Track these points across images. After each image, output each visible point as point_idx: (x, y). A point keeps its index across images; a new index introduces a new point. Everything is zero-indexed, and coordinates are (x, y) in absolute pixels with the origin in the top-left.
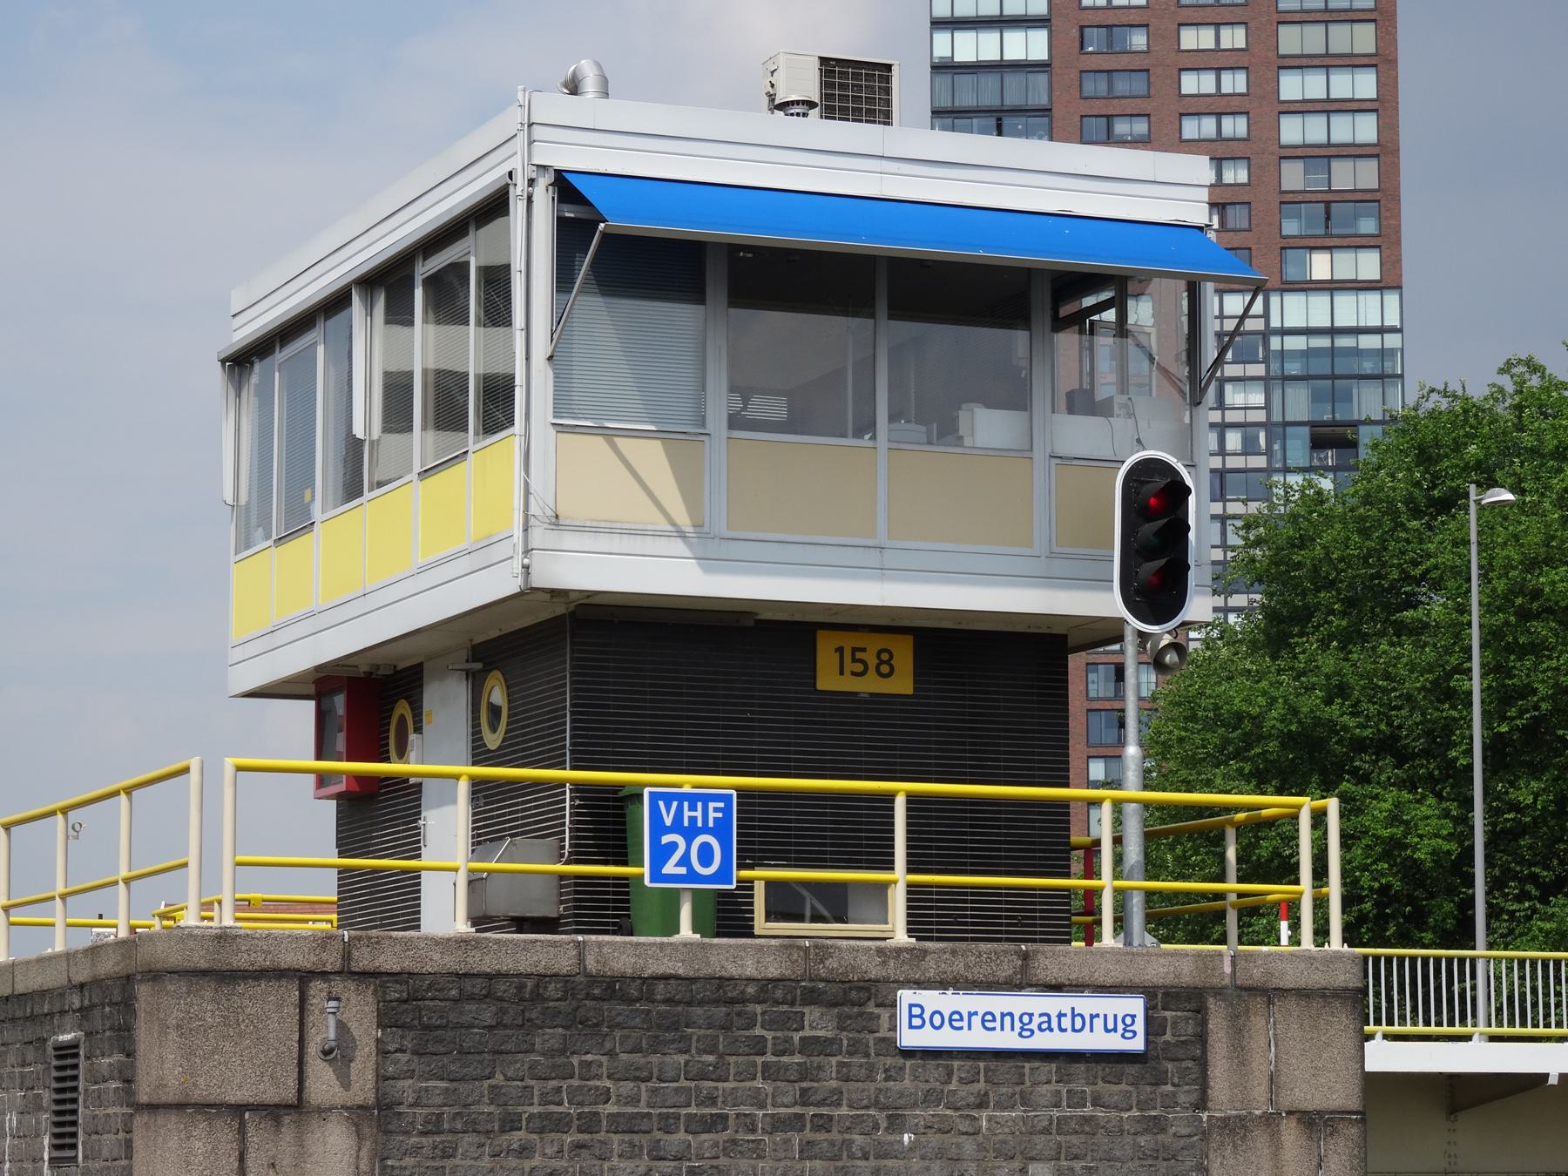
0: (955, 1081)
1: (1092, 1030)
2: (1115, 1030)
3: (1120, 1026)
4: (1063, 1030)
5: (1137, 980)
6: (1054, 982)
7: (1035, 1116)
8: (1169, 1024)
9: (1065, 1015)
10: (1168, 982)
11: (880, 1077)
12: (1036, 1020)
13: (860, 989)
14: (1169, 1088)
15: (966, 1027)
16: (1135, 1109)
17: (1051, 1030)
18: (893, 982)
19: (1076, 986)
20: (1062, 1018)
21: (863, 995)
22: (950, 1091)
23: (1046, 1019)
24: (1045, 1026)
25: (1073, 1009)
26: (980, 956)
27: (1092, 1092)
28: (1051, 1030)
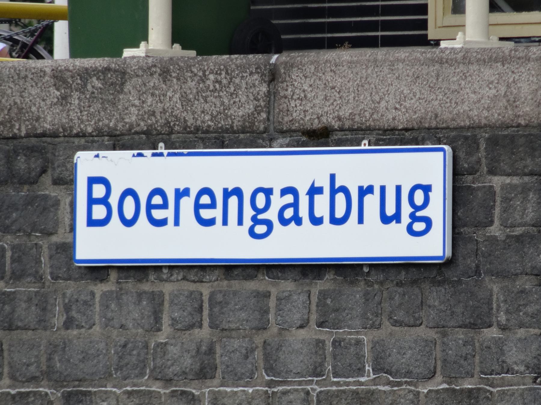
0: (166, 329)
1: (361, 221)
2: (397, 217)
3: (406, 210)
4: (316, 221)
5: (447, 116)
6: (316, 125)
7: (285, 393)
8: (498, 199)
9: (320, 190)
10: (495, 117)
11: (58, 320)
12: (277, 201)
13: (31, 150)
14: (493, 333)
15: (171, 221)
16: (439, 378)
17: (298, 221)
18: (77, 135)
19: (351, 130)
20: (317, 197)
21: (36, 164)
22: (158, 345)
23: (289, 199)
24: (289, 213)
25: (333, 177)
26: (203, 79)
27: (375, 344)
28: (298, 221)
